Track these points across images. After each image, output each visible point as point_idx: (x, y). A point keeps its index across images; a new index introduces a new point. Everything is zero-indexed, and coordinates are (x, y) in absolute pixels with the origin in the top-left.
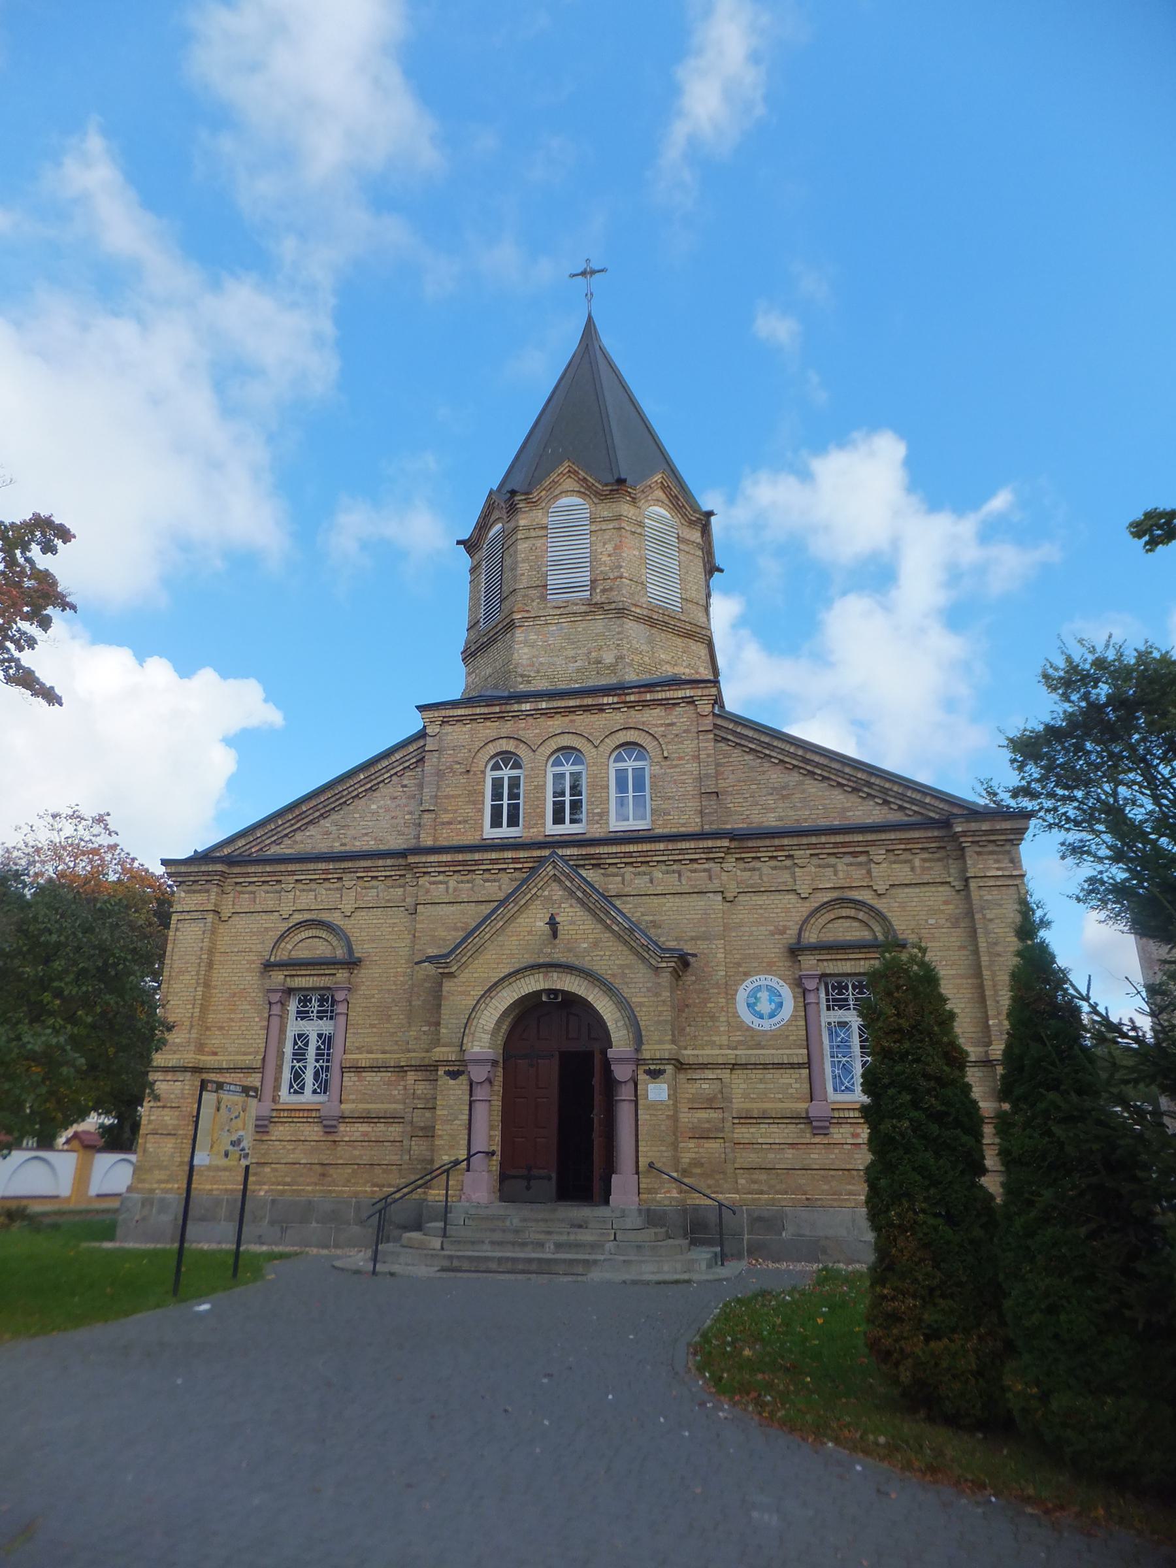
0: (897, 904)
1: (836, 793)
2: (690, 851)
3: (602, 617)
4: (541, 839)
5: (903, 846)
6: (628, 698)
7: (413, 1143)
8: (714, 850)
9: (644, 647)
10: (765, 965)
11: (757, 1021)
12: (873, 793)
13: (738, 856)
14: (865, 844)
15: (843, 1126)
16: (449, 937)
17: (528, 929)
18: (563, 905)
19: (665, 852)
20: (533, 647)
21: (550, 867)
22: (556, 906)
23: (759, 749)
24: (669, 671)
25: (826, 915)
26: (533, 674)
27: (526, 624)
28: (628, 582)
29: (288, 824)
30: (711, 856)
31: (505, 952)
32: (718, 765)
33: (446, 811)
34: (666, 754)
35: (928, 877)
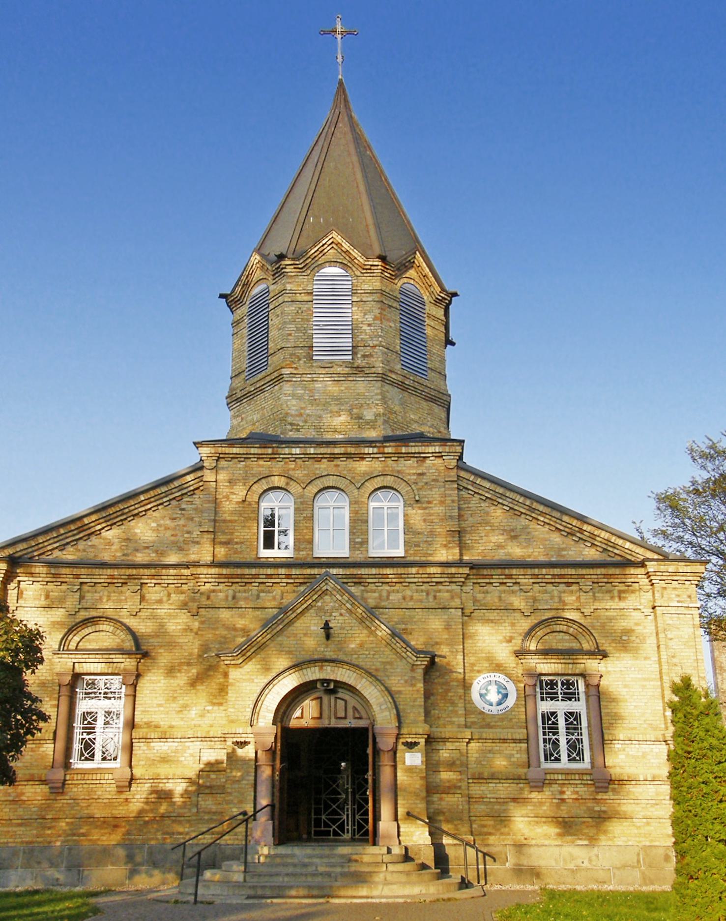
1: (555, 536)
2: (436, 576)
3: (363, 379)
4: (309, 560)
5: (605, 580)
7: (200, 799)
8: (456, 576)
10: (494, 665)
11: (487, 707)
12: (584, 538)
14: (576, 577)
15: (553, 786)
16: (229, 636)
17: (305, 632)
18: (334, 614)
21: (324, 584)
22: (328, 614)
23: (494, 498)
24: (416, 428)
25: (544, 629)
26: (301, 424)
27: (294, 379)
29: (70, 534)
30: (454, 580)
31: (284, 649)
32: (459, 509)
33: (224, 533)
34: (417, 498)
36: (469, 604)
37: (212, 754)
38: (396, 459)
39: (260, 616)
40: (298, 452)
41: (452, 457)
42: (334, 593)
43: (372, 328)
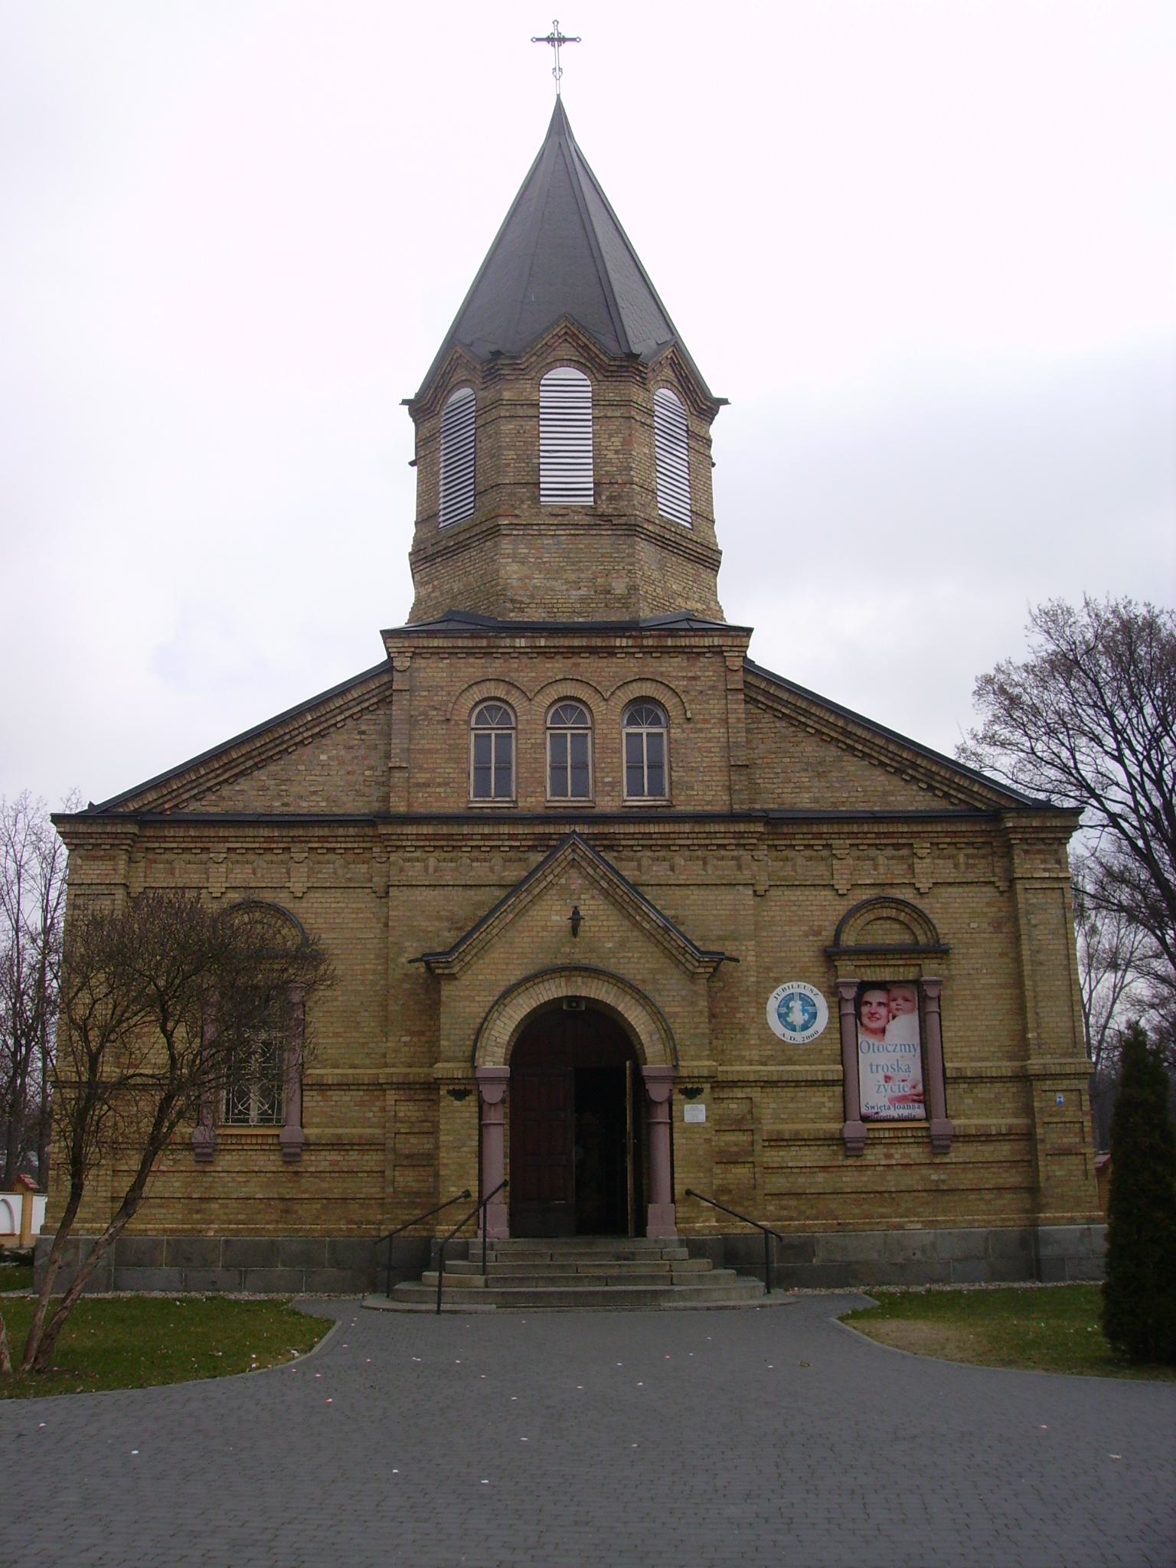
0: (939, 905)
1: (878, 773)
5: (948, 840)
9: (656, 575)
13: (770, 843)
18: (583, 896)
20: (523, 563)
23: (794, 715)
26: (524, 599)
27: (515, 532)
30: (742, 841)
31: (517, 950)
33: (421, 769)
34: (689, 715)
36: (762, 878)
37: (411, 1108)
38: (658, 655)
39: (474, 898)
40: (523, 645)
41: (737, 654)
42: (584, 864)
43: (621, 456)
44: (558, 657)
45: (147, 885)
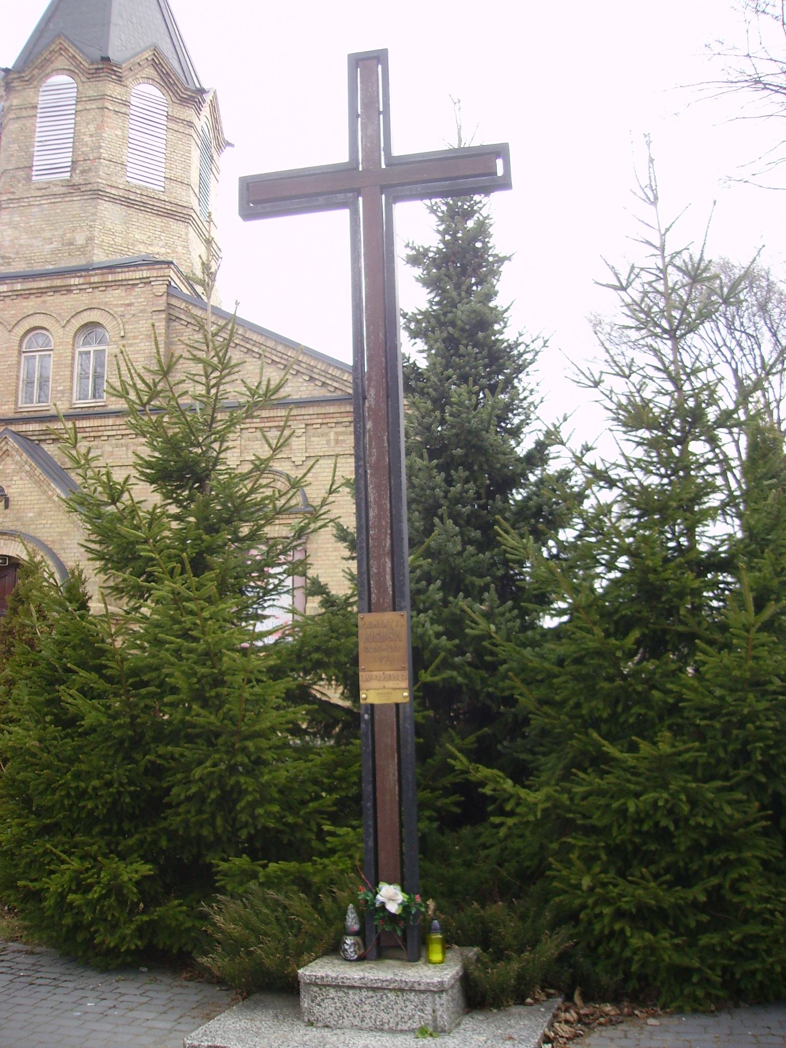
6: (93, 280)
9: (119, 228)
12: (301, 370)
18: (15, 478)
19: (114, 428)
20: (16, 228)
24: (143, 250)
26: (12, 256)
27: (11, 205)
28: (107, 162)
35: (340, 449)
44: (32, 297)
45: (307, 455)
